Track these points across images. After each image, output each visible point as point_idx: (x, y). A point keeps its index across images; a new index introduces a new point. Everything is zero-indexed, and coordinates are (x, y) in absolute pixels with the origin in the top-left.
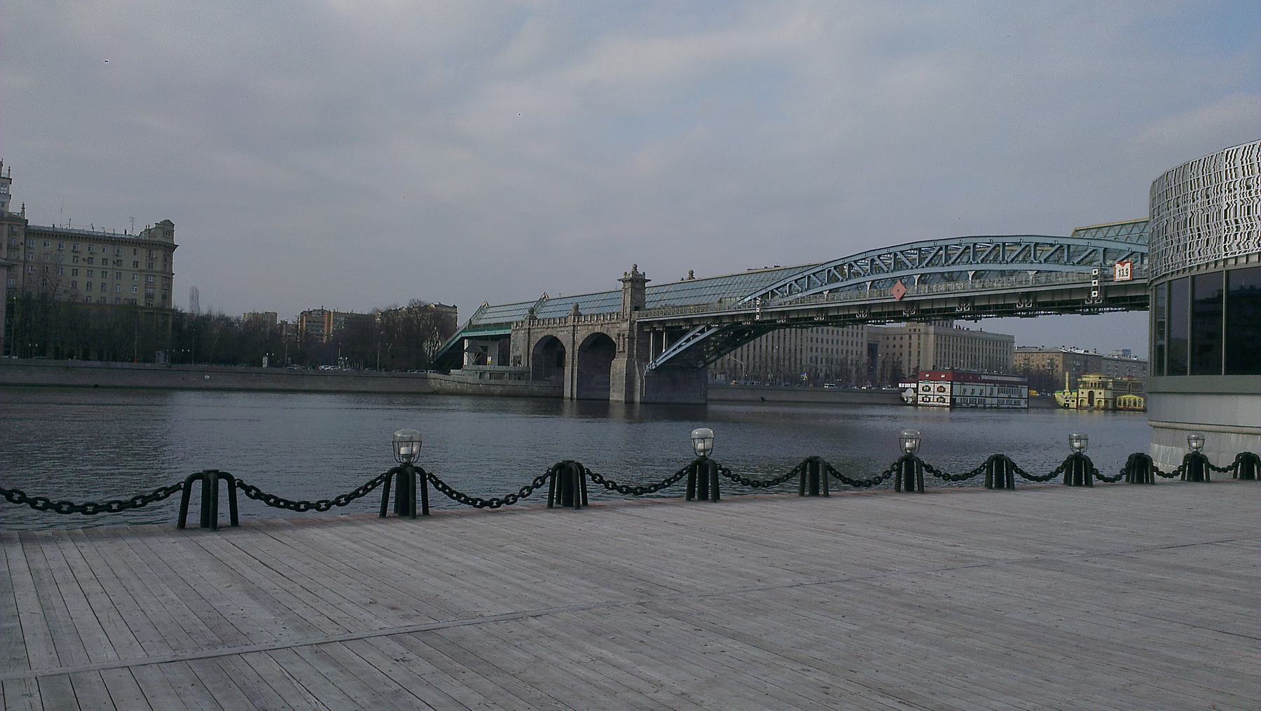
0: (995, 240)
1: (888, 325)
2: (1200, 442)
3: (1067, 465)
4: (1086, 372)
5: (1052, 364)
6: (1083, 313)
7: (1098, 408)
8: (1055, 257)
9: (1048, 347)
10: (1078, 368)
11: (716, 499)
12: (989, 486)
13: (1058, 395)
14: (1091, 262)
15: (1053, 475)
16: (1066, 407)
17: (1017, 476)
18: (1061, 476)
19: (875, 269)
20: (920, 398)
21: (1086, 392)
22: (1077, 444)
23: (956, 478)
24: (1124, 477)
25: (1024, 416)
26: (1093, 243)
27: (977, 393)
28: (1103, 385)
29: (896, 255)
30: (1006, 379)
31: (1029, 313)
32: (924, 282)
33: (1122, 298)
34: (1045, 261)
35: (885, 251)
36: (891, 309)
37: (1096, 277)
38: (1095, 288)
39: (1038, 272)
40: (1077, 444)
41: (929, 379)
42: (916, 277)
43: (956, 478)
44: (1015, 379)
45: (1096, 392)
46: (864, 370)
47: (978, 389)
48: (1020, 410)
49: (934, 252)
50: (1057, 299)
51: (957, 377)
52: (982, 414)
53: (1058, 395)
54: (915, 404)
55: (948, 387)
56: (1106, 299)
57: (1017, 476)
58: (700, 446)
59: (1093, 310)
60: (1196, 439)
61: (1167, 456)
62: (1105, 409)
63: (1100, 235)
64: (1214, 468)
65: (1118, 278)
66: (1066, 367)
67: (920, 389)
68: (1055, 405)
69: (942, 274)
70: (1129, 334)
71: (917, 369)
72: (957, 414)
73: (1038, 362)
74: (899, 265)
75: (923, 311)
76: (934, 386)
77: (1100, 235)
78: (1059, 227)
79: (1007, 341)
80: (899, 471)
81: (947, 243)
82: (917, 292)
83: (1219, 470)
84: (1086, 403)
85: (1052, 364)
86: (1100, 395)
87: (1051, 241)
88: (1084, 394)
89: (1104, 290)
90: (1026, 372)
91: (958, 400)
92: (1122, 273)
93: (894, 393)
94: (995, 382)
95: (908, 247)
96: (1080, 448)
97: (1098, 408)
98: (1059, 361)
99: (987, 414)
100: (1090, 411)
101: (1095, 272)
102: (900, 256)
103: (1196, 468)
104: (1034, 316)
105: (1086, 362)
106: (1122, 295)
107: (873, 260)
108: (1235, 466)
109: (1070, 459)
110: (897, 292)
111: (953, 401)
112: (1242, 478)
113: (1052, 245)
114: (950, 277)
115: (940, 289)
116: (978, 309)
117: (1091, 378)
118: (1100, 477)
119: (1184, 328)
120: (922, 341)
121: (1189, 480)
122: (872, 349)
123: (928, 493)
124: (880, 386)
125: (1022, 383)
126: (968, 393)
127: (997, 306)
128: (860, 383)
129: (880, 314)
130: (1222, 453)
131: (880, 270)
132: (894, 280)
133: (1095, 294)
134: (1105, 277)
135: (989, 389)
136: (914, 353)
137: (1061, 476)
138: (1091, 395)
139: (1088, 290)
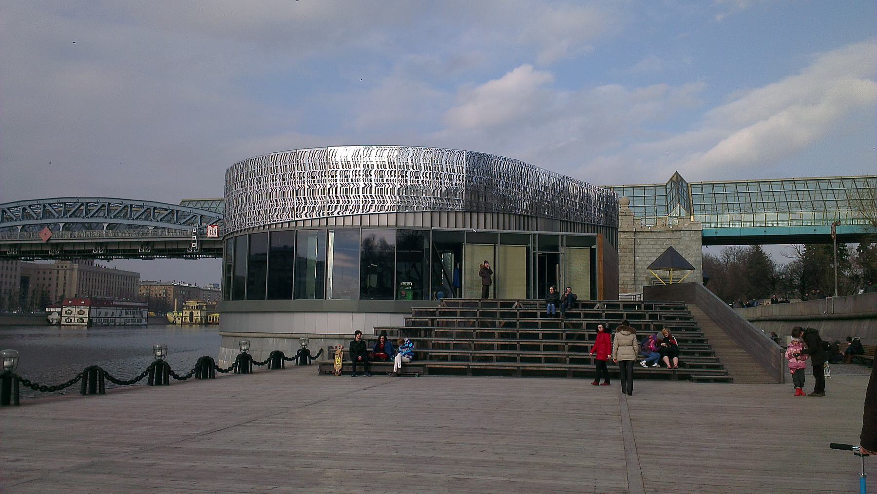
0: (125, 202)
1: (36, 262)
2: (247, 346)
3: (150, 370)
4: (189, 299)
5: (166, 293)
6: (186, 258)
7: (196, 323)
8: (168, 218)
9: (164, 281)
10: (184, 296)
11: (102, 392)
12: (83, 393)
13: (169, 315)
14: (192, 224)
15: (139, 379)
16: (174, 323)
17: (171, 378)
18: (146, 378)
19: (25, 215)
20: (63, 320)
21: (188, 312)
22: (159, 353)
23: (54, 389)
24: (194, 375)
25: (144, 330)
26: (194, 211)
27: (109, 315)
28: (200, 308)
29: (44, 206)
30: (132, 304)
31: (149, 257)
32: (68, 229)
33: (209, 249)
34: (161, 220)
35: (36, 203)
36: (39, 249)
37: (195, 234)
38: (194, 241)
39: (156, 227)
40: (159, 353)
41: (71, 305)
42: (62, 225)
43: (54, 389)
44: (139, 304)
45: (195, 312)
46: (17, 299)
47: (110, 311)
48: (140, 326)
49: (76, 207)
50: (168, 247)
51: (94, 303)
52: (113, 331)
53: (169, 315)
54: (59, 324)
55: (86, 311)
56: (201, 249)
57: (171, 378)
58: (6, 363)
59: (193, 256)
60: (245, 344)
61: (226, 357)
62: (201, 324)
63: (198, 206)
64: (256, 363)
65: (209, 235)
66: (176, 295)
67: (64, 312)
68: (167, 322)
69: (83, 224)
70: (208, 273)
71: (62, 297)
72: (93, 331)
73: (157, 292)
74: (47, 214)
75: (66, 251)
76: (75, 310)
77: (198, 206)
78: (173, 199)
79: (134, 277)
80: (85, 378)
81: (88, 200)
82: (62, 237)
83: (259, 364)
84: (188, 320)
85: (166, 293)
86: (197, 314)
87: (165, 207)
88: (187, 314)
89: (201, 243)
90: (148, 299)
91: (94, 320)
92: (212, 232)
93: (40, 316)
94: (123, 306)
95: (56, 201)
96: (161, 356)
97: (196, 323)
98: (171, 291)
99: (115, 331)
100: (191, 326)
101: (195, 230)
102: (48, 207)
103: (244, 364)
104: (152, 259)
105: (189, 292)
106: (212, 247)
107: (24, 209)
108: (297, 357)
109: (153, 365)
110: (45, 235)
111: (90, 321)
112: (273, 368)
113: (166, 210)
114: (89, 227)
115: (82, 235)
116: (110, 252)
117: (192, 303)
118: (176, 377)
119: (242, 270)
120: (68, 276)
121: (239, 373)
122: (25, 281)
123: (25, 404)
124: (29, 311)
125: (143, 307)
126: (102, 315)
127: (124, 251)
128: (12, 307)
129: (29, 252)
130: (261, 352)
131: (30, 217)
132: (42, 226)
133: (194, 245)
134: (201, 234)
135: (118, 311)
136: (61, 282)
137: (146, 378)
138: (191, 314)
139: (190, 243)
